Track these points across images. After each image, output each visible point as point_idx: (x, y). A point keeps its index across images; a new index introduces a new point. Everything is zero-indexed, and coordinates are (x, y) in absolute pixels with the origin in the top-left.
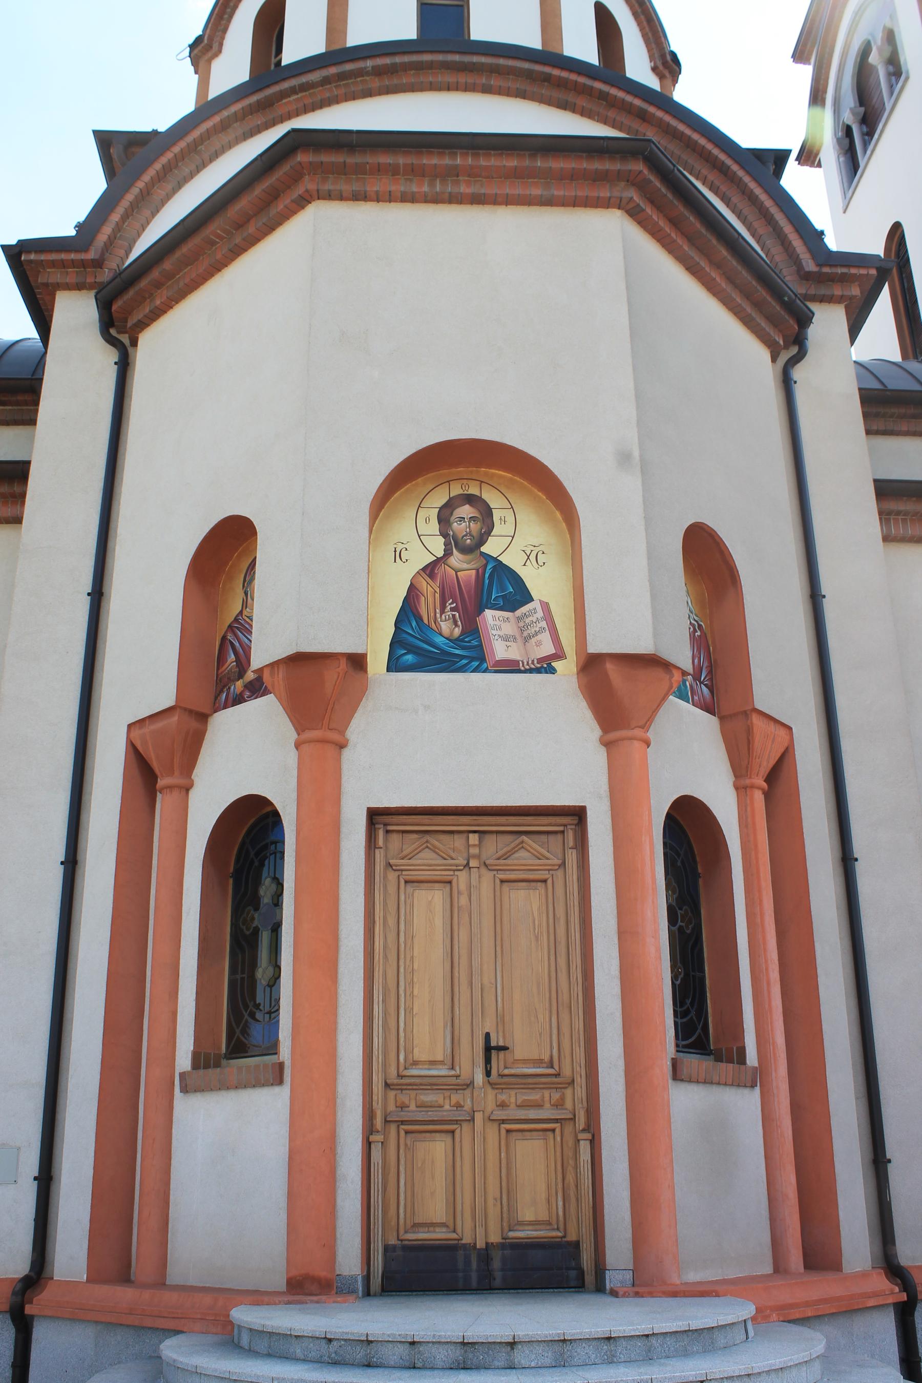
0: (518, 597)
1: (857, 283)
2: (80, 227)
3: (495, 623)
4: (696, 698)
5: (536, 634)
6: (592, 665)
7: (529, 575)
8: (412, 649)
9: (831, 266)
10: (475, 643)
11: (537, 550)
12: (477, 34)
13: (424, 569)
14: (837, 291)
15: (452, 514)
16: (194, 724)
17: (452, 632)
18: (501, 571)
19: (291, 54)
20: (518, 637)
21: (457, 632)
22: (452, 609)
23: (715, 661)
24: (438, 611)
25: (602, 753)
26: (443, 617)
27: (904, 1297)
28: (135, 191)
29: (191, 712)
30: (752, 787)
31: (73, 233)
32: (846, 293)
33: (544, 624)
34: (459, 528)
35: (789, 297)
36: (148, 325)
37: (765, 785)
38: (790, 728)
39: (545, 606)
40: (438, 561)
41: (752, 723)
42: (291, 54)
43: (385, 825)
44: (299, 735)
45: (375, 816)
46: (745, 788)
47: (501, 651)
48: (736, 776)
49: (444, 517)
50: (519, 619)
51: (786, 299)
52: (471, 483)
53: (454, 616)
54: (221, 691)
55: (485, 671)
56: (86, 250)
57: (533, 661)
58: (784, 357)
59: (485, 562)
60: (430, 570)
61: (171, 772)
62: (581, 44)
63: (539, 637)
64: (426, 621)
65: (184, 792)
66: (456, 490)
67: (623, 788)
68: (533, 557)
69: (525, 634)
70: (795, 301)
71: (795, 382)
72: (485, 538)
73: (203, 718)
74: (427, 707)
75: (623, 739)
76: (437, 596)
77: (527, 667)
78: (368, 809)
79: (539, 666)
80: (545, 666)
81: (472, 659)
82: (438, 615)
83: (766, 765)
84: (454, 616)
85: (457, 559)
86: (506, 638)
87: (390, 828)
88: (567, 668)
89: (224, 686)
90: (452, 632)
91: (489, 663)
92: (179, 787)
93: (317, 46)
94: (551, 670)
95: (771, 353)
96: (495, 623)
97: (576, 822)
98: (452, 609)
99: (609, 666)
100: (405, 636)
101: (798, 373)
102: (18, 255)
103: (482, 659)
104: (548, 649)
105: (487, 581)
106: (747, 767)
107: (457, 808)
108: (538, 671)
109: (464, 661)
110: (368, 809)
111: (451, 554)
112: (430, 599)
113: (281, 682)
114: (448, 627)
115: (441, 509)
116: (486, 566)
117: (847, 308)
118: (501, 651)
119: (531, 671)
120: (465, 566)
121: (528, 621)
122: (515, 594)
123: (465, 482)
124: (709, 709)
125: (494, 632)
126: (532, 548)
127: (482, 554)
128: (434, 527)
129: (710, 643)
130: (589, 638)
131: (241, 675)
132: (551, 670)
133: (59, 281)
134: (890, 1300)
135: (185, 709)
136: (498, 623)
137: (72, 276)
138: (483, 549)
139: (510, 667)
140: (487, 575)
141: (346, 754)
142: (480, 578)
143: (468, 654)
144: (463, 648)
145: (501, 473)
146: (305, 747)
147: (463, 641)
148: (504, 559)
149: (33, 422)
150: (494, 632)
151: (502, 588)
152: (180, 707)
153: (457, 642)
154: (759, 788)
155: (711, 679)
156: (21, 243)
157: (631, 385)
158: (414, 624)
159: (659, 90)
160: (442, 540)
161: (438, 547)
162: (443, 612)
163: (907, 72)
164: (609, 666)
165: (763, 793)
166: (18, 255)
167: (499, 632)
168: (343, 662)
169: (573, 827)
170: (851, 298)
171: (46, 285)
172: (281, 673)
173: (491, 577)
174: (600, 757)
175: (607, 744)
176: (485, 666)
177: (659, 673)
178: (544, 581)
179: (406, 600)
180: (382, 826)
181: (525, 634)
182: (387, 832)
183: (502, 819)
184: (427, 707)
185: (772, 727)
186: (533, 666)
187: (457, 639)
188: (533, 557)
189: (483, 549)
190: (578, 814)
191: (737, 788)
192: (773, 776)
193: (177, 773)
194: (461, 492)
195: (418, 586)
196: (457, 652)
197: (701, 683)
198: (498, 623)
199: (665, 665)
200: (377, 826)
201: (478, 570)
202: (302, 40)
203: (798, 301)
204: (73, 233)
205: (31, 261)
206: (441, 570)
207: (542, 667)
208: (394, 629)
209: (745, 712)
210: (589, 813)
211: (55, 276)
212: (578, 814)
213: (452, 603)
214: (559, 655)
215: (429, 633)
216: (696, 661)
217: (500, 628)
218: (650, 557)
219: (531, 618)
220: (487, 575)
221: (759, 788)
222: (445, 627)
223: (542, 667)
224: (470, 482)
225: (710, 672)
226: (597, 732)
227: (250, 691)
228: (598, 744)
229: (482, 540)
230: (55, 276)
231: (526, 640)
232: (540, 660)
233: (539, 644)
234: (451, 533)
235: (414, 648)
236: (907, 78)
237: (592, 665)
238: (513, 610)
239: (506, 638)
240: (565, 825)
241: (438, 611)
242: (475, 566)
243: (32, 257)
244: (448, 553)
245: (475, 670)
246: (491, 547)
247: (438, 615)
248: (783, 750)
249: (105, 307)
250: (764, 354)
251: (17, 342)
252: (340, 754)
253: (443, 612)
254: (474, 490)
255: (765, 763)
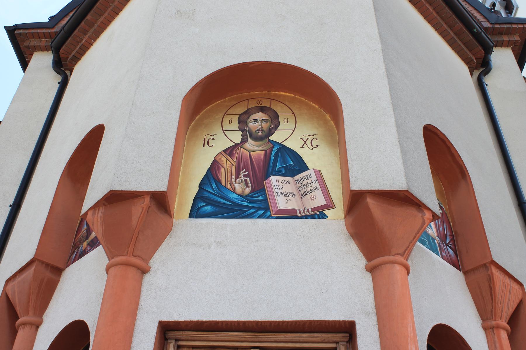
0: (297, 168)
1: (517, 34)
2: (51, 18)
3: (278, 184)
4: (444, 254)
5: (311, 191)
6: (356, 200)
7: (307, 155)
8: (209, 202)
9: (499, 24)
10: (261, 198)
11: (312, 138)
13: (225, 151)
14: (506, 38)
15: (249, 118)
16: (48, 274)
17: (243, 191)
18: (283, 150)
20: (296, 193)
21: (248, 191)
22: (244, 176)
23: (456, 232)
24: (233, 177)
25: (368, 277)
26: (237, 181)
29: (47, 265)
30: (498, 327)
31: (48, 20)
32: (511, 39)
33: (317, 185)
34: (252, 126)
35: (477, 30)
36: (79, 59)
37: (508, 327)
38: (521, 285)
39: (319, 173)
40: (236, 145)
41: (492, 273)
43: (177, 340)
44: (109, 260)
45: (167, 330)
46: (492, 328)
47: (282, 203)
48: (482, 319)
49: (242, 121)
50: (297, 182)
51: (475, 30)
52: (264, 101)
53: (246, 180)
54: (74, 251)
55: (268, 218)
57: (308, 210)
58: (477, 73)
59: (272, 146)
60: (229, 152)
61: (27, 313)
63: (313, 193)
64: (223, 183)
65: (34, 328)
66: (253, 104)
67: (389, 309)
68: (309, 142)
69: (302, 191)
70: (481, 33)
71: (487, 85)
72: (273, 131)
73: (58, 271)
74: (219, 243)
75: (385, 263)
76: (234, 167)
77: (303, 214)
78: (160, 323)
79: (313, 213)
80: (319, 213)
81: (259, 209)
82: (233, 180)
83: (507, 310)
84: (246, 180)
85: (250, 144)
86: (287, 195)
87: (181, 343)
88: (336, 215)
89: (76, 248)
90: (243, 191)
91: (273, 211)
92: (31, 324)
94: (324, 216)
95: (469, 68)
96: (278, 184)
97: (347, 339)
98: (244, 176)
99: (370, 201)
100: (206, 193)
101: (488, 80)
102: (15, 33)
103: (267, 209)
104: (320, 200)
105: (273, 158)
106: (492, 311)
107: (239, 322)
108: (312, 217)
109: (252, 211)
110: (160, 323)
111: (247, 141)
112: (228, 170)
113: (99, 220)
114: (240, 187)
115: (241, 115)
116: (272, 148)
117: (513, 50)
118: (282, 203)
119: (306, 217)
120: (257, 148)
121: (304, 183)
122: (294, 166)
123: (260, 99)
124: (456, 265)
125: (277, 191)
126: (308, 137)
127: (270, 141)
128: (235, 125)
129: (450, 220)
130: (352, 179)
131: (87, 238)
132: (324, 216)
133: (36, 45)
135: (43, 262)
136: (280, 184)
137: (43, 42)
138: (271, 138)
139: (290, 214)
140: (273, 154)
141: (147, 278)
142: (267, 156)
143: (257, 205)
144: (252, 201)
145: (286, 94)
146: (112, 270)
147: (252, 196)
148: (287, 144)
150: (277, 191)
151: (284, 161)
152: (38, 260)
153: (247, 197)
154: (504, 329)
155: (454, 244)
157: (377, 32)
158: (214, 185)
160: (240, 133)
161: (237, 137)
162: (237, 177)
163: (517, 5)
164: (370, 201)
165: (508, 334)
166: (15, 33)
167: (281, 191)
168: (147, 199)
169: (345, 344)
170: (515, 42)
171: (28, 47)
172: (100, 213)
173: (276, 155)
174: (365, 282)
175: (371, 269)
176: (269, 213)
177: (413, 211)
178: (317, 158)
179: (209, 170)
180: (174, 341)
181: (302, 191)
182: (179, 347)
183: (281, 336)
184: (219, 243)
185: (507, 280)
186: (308, 214)
187: (248, 195)
188: (309, 142)
189: (271, 138)
190: (348, 330)
191: (485, 329)
192: (514, 320)
193: (31, 313)
194: (257, 105)
195: (219, 161)
196: (247, 204)
197: (447, 245)
198: (280, 184)
199: (419, 205)
200: (169, 341)
201: (266, 151)
203: (483, 33)
204: (48, 20)
205: (20, 34)
206: (237, 152)
207: (316, 214)
208: (197, 189)
209: (485, 265)
210: (358, 327)
211: (33, 42)
212: (348, 330)
213: (245, 172)
214: (330, 205)
215: (225, 192)
216: (441, 229)
217: (282, 188)
218: (398, 127)
219: (307, 181)
220: (273, 154)
221: (504, 329)
222: (239, 188)
223: (316, 214)
224: (263, 100)
225: (452, 240)
226: (363, 261)
227: (90, 246)
228: (364, 270)
229: (270, 133)
230: (33, 42)
231: (303, 196)
232: (313, 209)
233: (313, 198)
234: (248, 129)
235: (212, 202)
236: (517, 8)
237: (356, 200)
238: (293, 176)
239: (287, 195)
240: (337, 343)
241: (233, 177)
242: (264, 148)
243: (21, 31)
244: (244, 140)
245: (260, 217)
246: (276, 137)
247: (233, 180)
248: (518, 301)
249: (56, 51)
250: (464, 68)
252: (142, 279)
253: (237, 177)
254: (266, 104)
255: (506, 309)
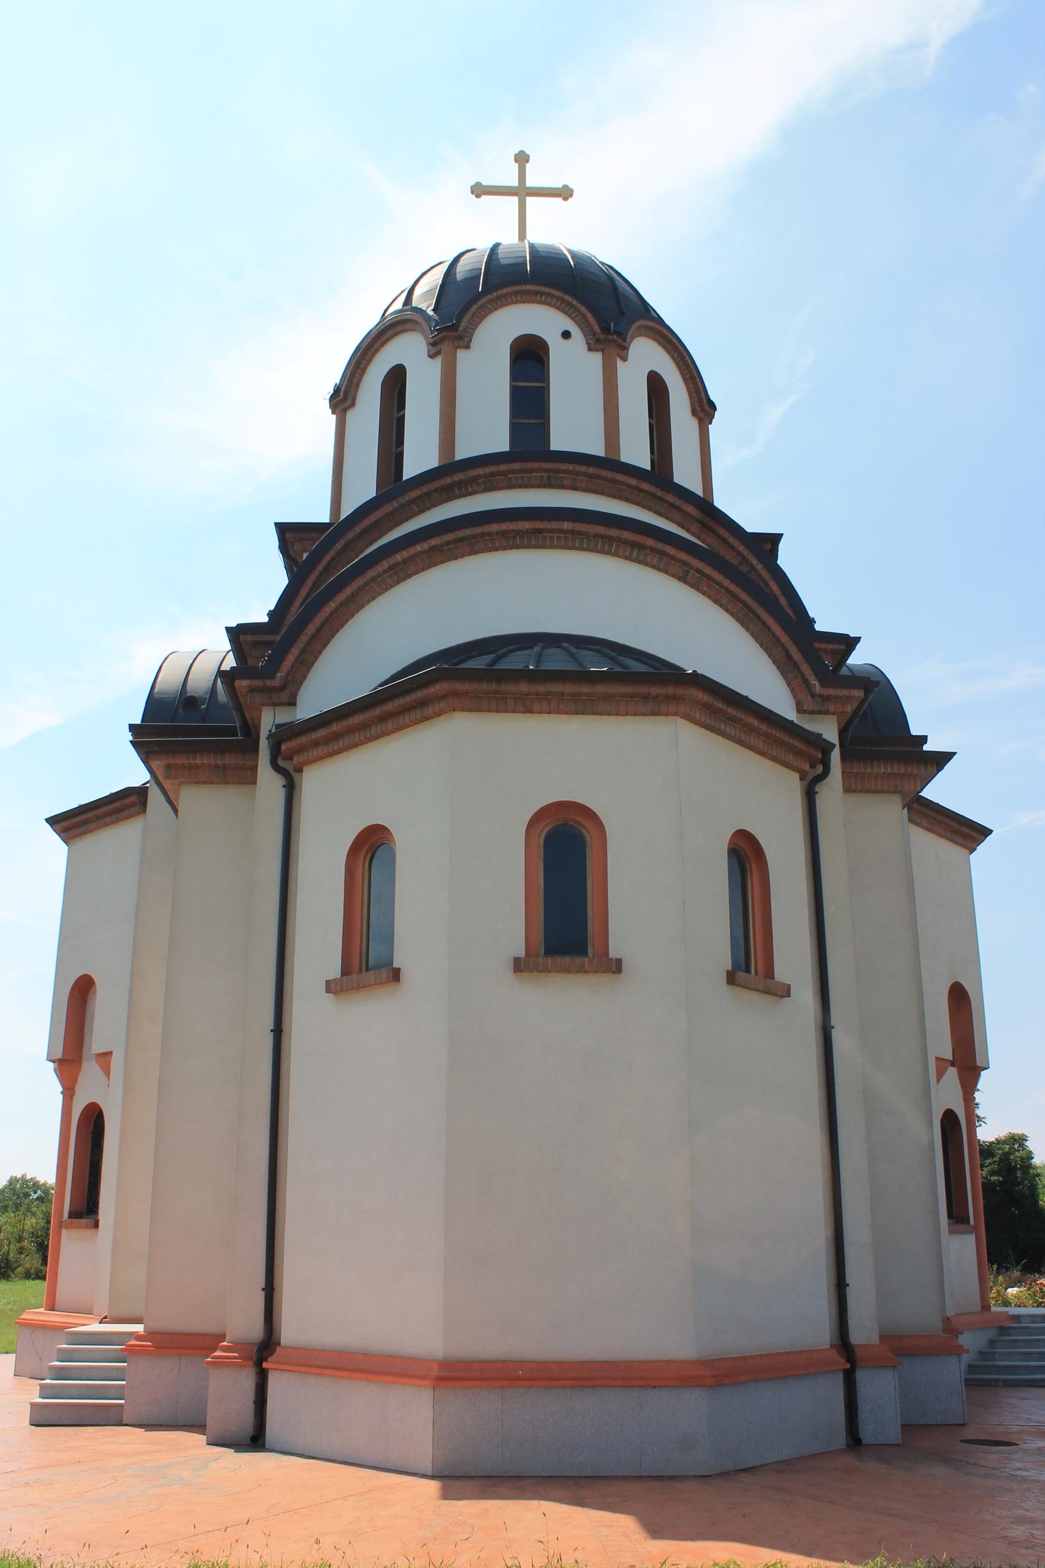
2: (271, 614)
12: (553, 447)
19: (409, 471)
27: (848, 1366)
28: (537, 288)
31: (266, 619)
42: (409, 471)
56: (272, 676)
62: (636, 451)
93: (432, 462)
134: (842, 1367)
149: (255, 783)
156: (240, 627)
159: (701, 494)
202: (420, 456)
204: (266, 619)
251: (457, 260)
